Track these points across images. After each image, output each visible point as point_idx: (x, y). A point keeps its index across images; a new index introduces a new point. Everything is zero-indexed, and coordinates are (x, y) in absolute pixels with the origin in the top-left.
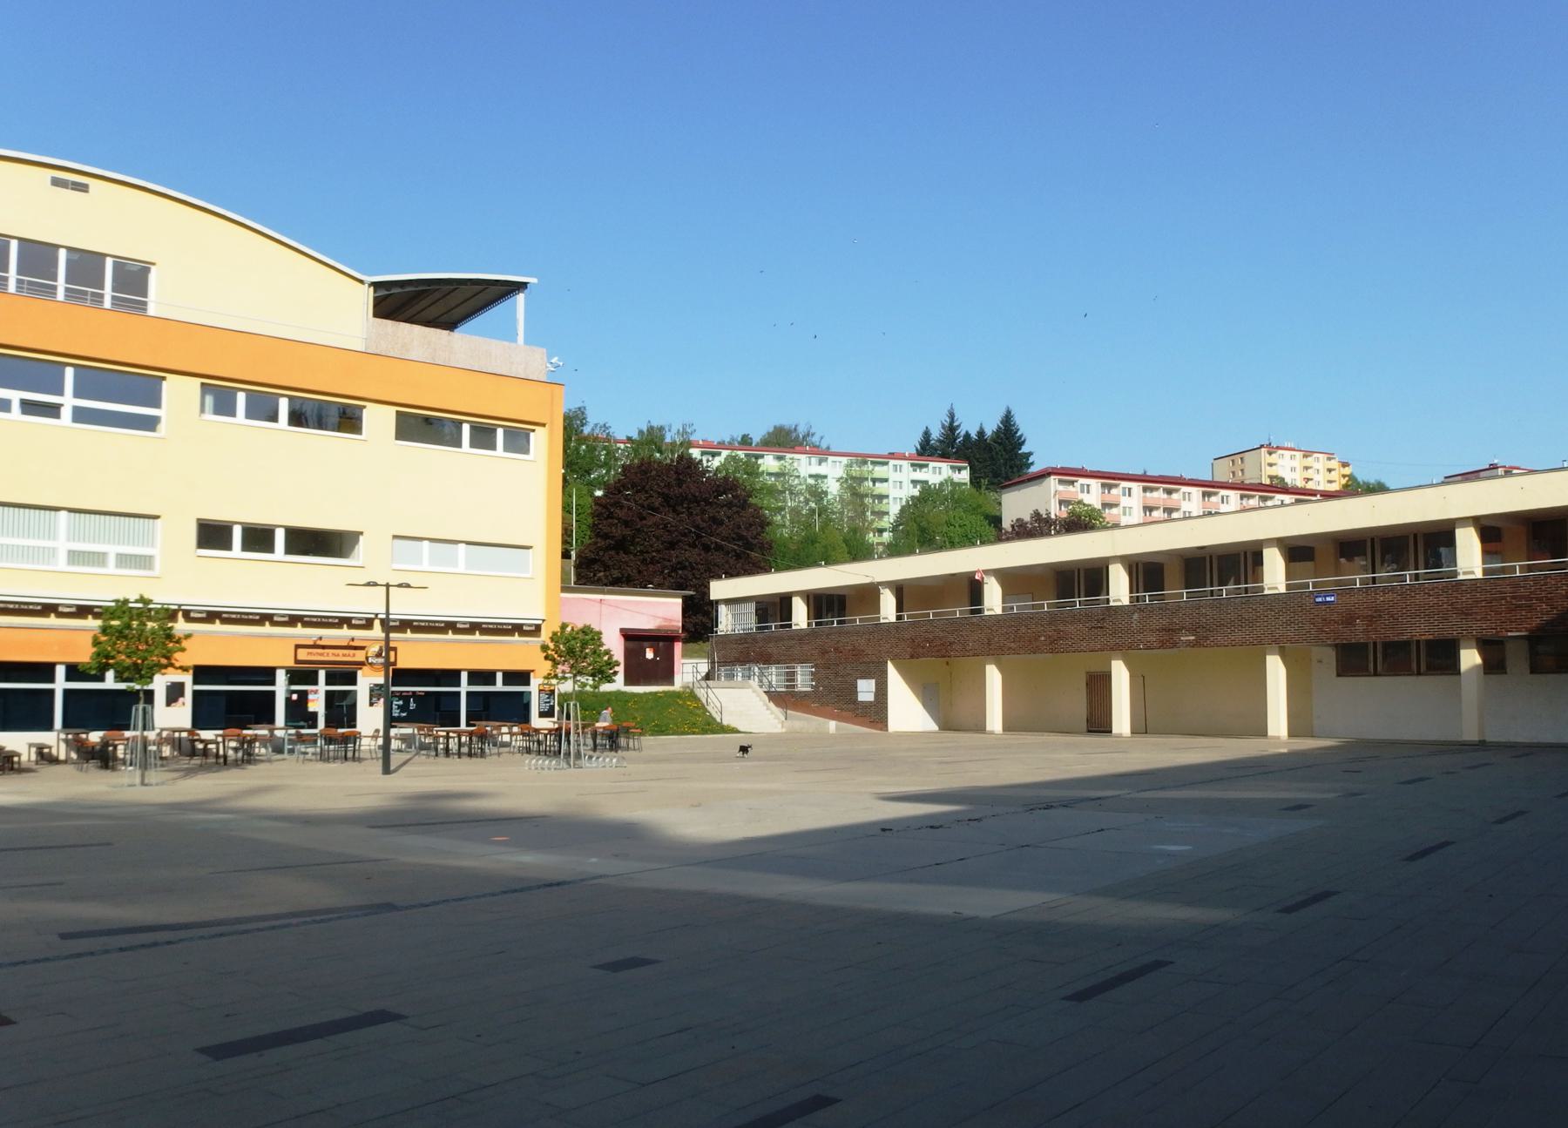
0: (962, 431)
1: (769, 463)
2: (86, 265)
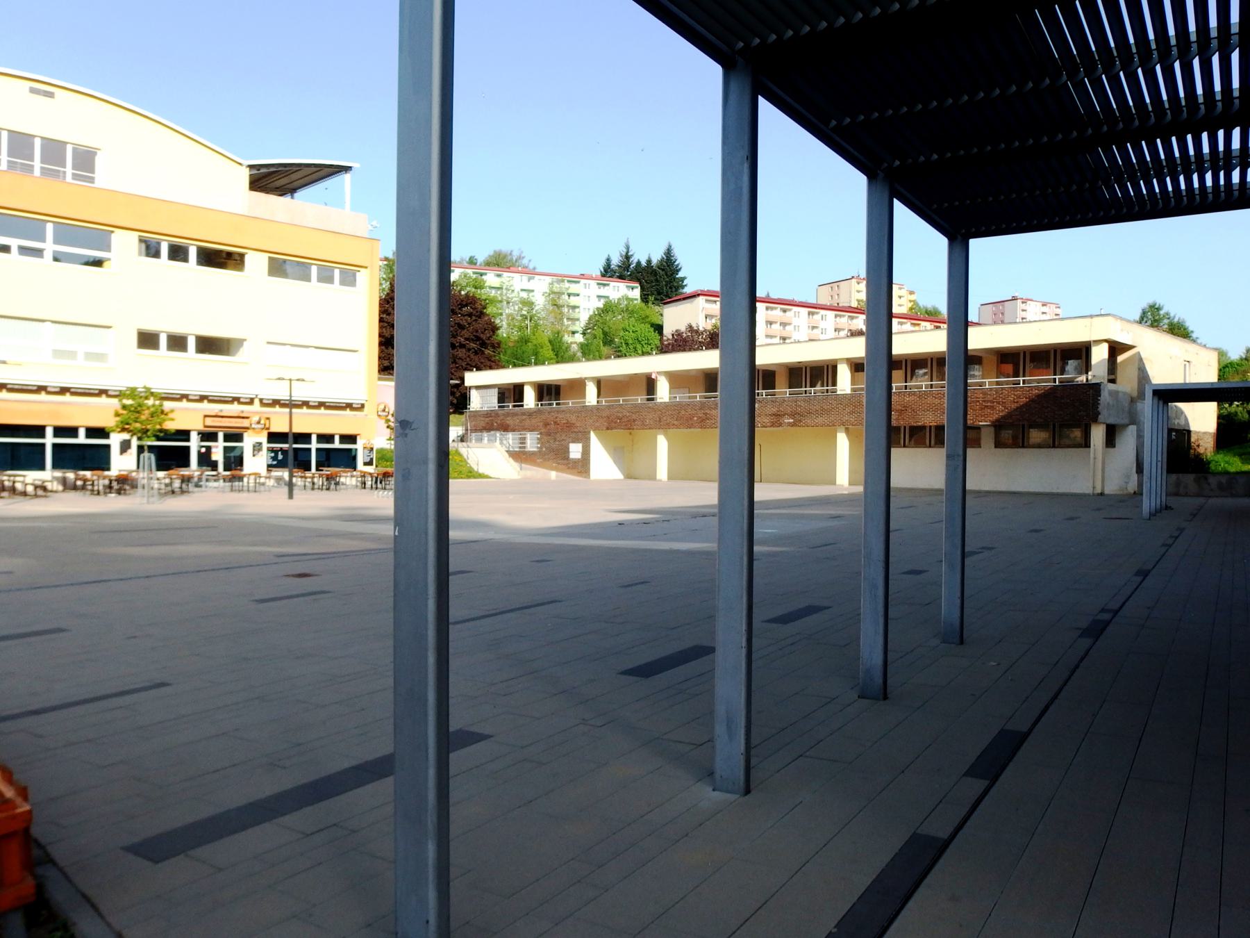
0: (634, 260)
1: (491, 279)
2: (54, 150)
